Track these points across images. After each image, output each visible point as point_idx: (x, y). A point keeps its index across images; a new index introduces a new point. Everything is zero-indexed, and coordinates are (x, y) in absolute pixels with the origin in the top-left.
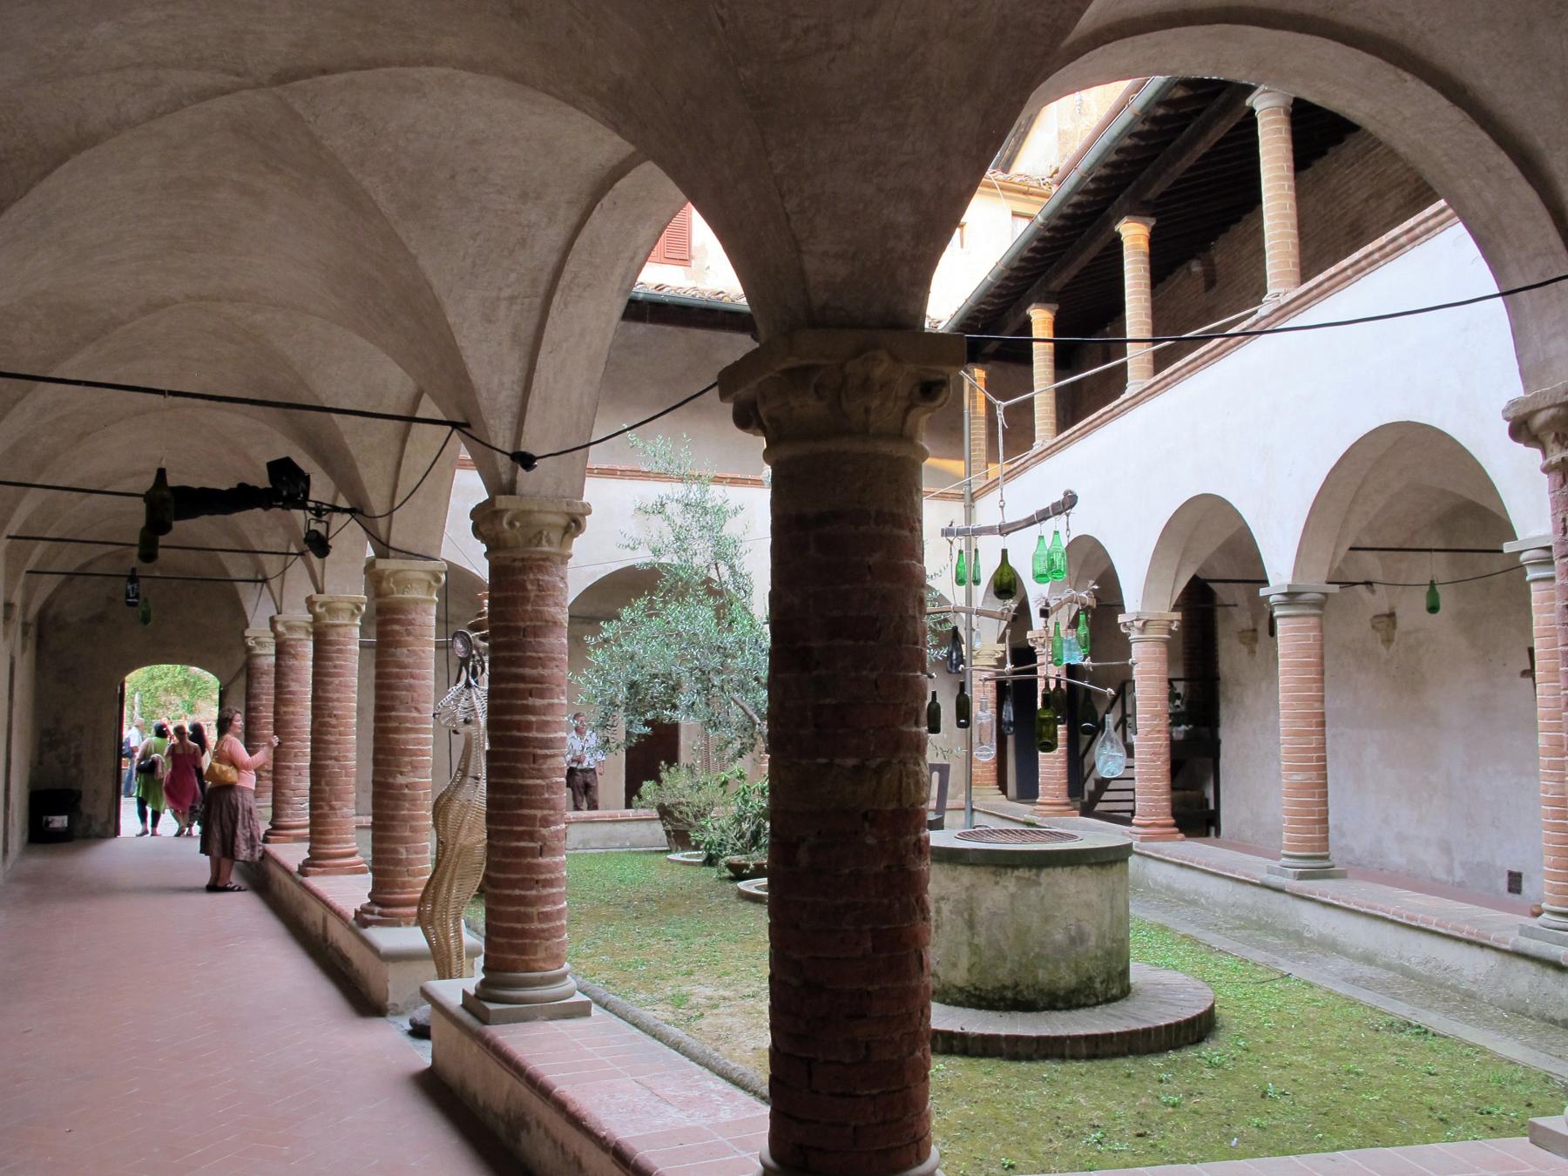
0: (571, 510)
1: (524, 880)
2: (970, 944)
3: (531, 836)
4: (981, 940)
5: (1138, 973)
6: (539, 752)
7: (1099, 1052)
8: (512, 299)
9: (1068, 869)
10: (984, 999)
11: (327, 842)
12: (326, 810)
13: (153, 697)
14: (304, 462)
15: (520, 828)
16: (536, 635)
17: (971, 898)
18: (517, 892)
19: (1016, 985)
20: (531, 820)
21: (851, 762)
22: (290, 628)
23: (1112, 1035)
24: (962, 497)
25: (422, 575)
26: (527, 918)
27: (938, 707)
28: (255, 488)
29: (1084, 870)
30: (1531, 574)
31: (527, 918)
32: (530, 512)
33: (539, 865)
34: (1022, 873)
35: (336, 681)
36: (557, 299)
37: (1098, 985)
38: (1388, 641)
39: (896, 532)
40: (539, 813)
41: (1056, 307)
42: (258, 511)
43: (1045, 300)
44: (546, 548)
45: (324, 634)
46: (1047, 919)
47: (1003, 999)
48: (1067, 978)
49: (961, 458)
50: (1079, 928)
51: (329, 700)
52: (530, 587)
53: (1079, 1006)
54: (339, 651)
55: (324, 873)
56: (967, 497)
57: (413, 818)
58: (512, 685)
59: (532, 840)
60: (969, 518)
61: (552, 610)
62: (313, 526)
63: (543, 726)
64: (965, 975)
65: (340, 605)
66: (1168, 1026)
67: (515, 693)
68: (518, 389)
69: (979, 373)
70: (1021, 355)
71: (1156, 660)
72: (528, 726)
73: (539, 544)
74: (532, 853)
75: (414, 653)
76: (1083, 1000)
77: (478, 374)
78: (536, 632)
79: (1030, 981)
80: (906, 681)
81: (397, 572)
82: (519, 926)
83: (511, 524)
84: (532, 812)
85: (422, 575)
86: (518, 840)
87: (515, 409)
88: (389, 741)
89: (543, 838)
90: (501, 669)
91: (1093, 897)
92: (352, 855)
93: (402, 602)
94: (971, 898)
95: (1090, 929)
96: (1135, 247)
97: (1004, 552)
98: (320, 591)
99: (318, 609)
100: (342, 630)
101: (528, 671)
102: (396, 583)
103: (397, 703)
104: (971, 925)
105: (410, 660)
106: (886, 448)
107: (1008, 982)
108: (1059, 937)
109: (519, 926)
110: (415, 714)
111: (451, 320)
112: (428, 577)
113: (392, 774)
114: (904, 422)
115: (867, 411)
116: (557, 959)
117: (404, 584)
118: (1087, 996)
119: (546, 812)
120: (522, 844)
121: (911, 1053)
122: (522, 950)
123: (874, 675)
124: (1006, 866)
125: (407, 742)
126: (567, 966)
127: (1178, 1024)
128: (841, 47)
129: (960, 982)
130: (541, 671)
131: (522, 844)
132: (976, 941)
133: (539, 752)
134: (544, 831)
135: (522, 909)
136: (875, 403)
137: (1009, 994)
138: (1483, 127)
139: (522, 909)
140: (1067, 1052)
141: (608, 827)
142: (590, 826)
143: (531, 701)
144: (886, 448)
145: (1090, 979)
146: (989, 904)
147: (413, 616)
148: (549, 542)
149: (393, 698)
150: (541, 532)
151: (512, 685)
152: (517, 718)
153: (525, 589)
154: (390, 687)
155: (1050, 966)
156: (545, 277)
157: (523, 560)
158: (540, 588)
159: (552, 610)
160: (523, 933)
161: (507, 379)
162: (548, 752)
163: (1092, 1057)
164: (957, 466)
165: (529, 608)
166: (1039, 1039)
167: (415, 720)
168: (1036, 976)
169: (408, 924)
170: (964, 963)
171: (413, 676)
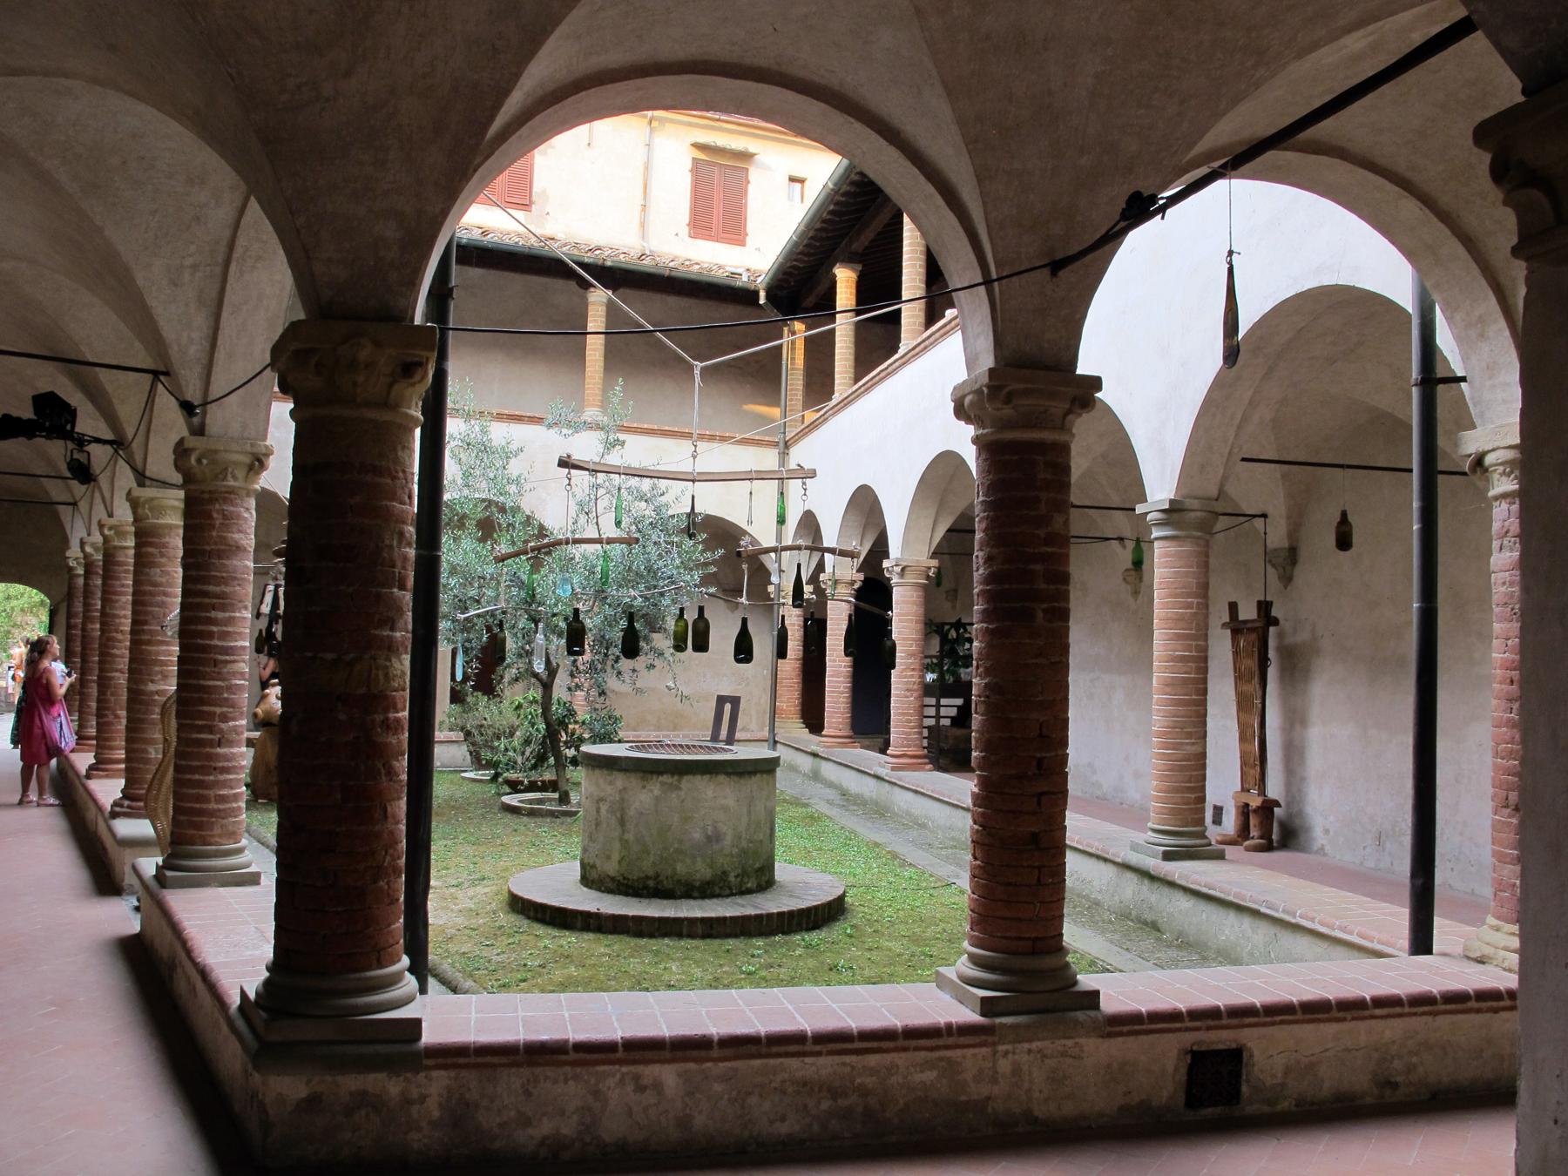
0: (255, 450)
1: (202, 767)
3: (211, 729)
4: (630, 837)
5: (782, 871)
8: (195, 267)
10: (632, 887)
12: (111, 718)
13: (9, 616)
14: (74, 398)
16: (220, 558)
17: (623, 800)
18: (197, 777)
19: (657, 875)
20: (212, 715)
21: (330, 656)
23: (725, 919)
24: (776, 444)
26: (206, 799)
28: (19, 419)
29: (722, 778)
30: (1156, 533)
31: (206, 799)
32: (216, 452)
33: (218, 755)
34: (666, 778)
36: (233, 267)
37: (732, 878)
38: (1136, 593)
39: (378, 480)
40: (218, 710)
42: (22, 439)
43: (849, 260)
44: (232, 483)
45: (113, 556)
46: (686, 820)
47: (646, 887)
48: (702, 871)
49: (778, 405)
51: (115, 616)
55: (107, 777)
58: (198, 600)
60: (782, 463)
61: (236, 536)
62: (76, 456)
63: (225, 635)
66: (781, 914)
67: (200, 607)
68: (207, 345)
70: (826, 305)
72: (211, 635)
73: (225, 478)
74: (211, 744)
75: (168, 573)
76: (717, 891)
77: (169, 332)
78: (220, 555)
79: (669, 872)
80: (378, 596)
83: (199, 461)
84: (212, 709)
87: (204, 362)
88: (142, 652)
89: (221, 731)
90: (190, 586)
91: (730, 802)
94: (623, 800)
95: (728, 831)
98: (111, 515)
99: (106, 532)
101: (211, 588)
102: (151, 509)
103: (149, 618)
104: (622, 822)
105: (164, 580)
106: (371, 414)
107: (651, 873)
108: (697, 835)
111: (140, 282)
113: (142, 682)
114: (389, 393)
115: (355, 384)
116: (233, 836)
121: (375, 882)
122: (200, 826)
123: (351, 589)
124: (652, 773)
125: (158, 653)
126: (244, 842)
127: (791, 913)
128: (328, 100)
129: (612, 873)
130: (224, 588)
132: (626, 836)
134: (223, 726)
136: (361, 379)
137: (651, 883)
138: (914, 164)
140: (685, 931)
143: (213, 614)
144: (371, 414)
145: (724, 873)
146: (637, 804)
148: (235, 478)
149: (146, 613)
151: (198, 600)
152: (200, 627)
153: (210, 517)
154: (143, 604)
156: (222, 249)
158: (225, 517)
159: (236, 536)
160: (201, 812)
161: (195, 335)
164: (776, 412)
166: (661, 919)
170: (616, 857)
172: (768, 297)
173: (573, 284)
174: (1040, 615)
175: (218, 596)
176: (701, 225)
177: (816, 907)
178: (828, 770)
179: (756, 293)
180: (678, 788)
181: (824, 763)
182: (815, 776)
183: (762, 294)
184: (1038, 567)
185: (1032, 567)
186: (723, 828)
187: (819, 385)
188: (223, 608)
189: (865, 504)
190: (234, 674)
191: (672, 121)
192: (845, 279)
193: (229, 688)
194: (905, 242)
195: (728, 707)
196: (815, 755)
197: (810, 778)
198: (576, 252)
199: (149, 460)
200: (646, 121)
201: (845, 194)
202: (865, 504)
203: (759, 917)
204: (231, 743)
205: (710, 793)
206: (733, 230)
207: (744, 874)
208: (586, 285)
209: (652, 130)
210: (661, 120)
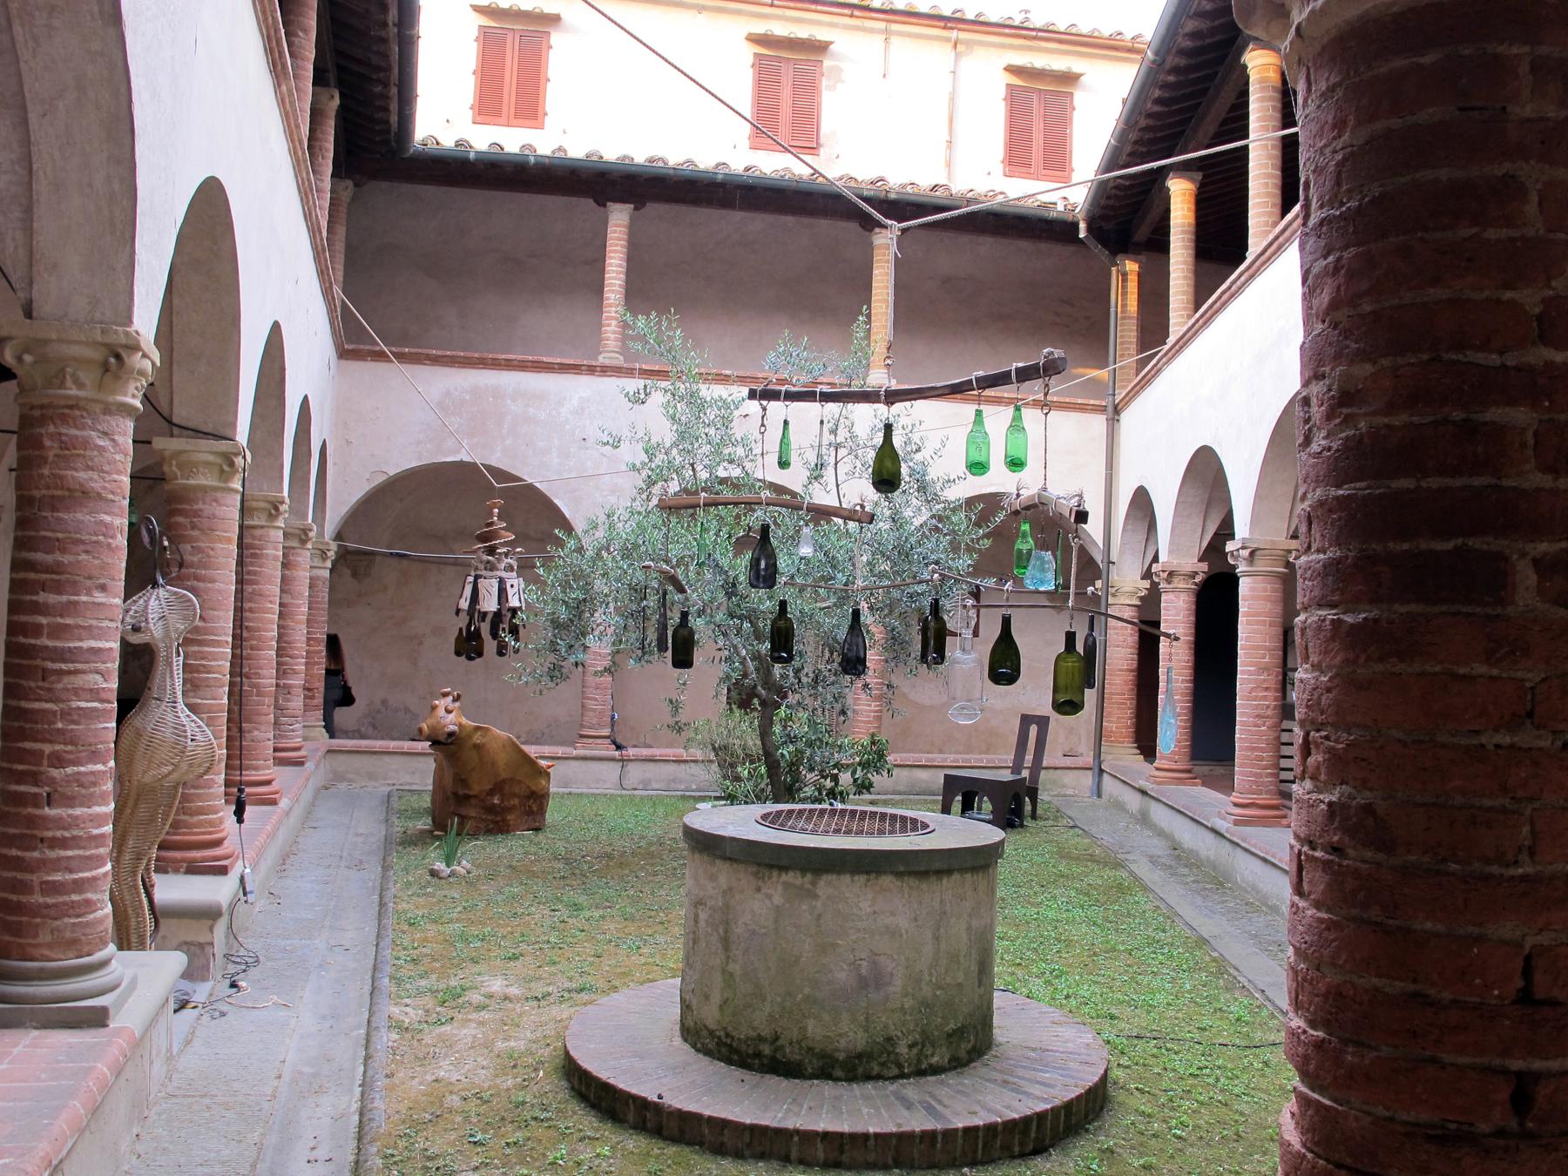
0: (107, 340)
1: (23, 836)
2: (724, 971)
5: (1018, 1018)
6: (50, 665)
7: (845, 1158)
9: (862, 879)
10: (737, 1051)
15: (20, 767)
16: (54, 509)
18: (14, 852)
23: (866, 1136)
24: (1101, 409)
25: (211, 458)
26: (25, 888)
27: (692, 633)
29: (887, 880)
31: (25, 888)
32: (46, 342)
33: (45, 818)
34: (791, 877)
37: (902, 1049)
40: (47, 748)
41: (1199, 176)
43: (1184, 168)
44: (74, 392)
47: (758, 1055)
48: (850, 1036)
52: (48, 443)
53: (868, 1077)
54: (254, 556)
56: (1110, 409)
59: (36, 784)
61: (82, 475)
63: (59, 631)
64: (717, 1014)
65: (255, 504)
66: (970, 1131)
69: (1131, 266)
71: (1266, 599)
72: (59, 631)
73: (62, 385)
74: (35, 801)
75: (199, 550)
76: (876, 1069)
79: (795, 1035)
81: (181, 452)
82: (14, 898)
85: (211, 458)
86: (18, 783)
89: (53, 781)
92: (268, 783)
93: (187, 488)
96: (1262, 80)
97: (888, 428)
100: (258, 532)
101: (39, 556)
102: (179, 466)
104: (726, 942)
105: (195, 559)
107: (766, 1032)
108: (842, 975)
109: (14, 898)
112: (219, 460)
117: (189, 467)
118: (883, 1064)
119: (58, 747)
120: (22, 788)
122: (17, 930)
124: (771, 867)
127: (991, 1129)
130: (58, 556)
131: (22, 788)
132: (731, 967)
133: (50, 665)
135: (19, 876)
137: (766, 1050)
139: (19, 876)
140: (794, 1154)
141: (672, 768)
142: (651, 766)
143: (42, 597)
145: (889, 1039)
147: (200, 506)
150: (63, 370)
153: (41, 446)
155: (826, 1017)
157: (42, 407)
158: (64, 446)
159: (82, 475)
160: (19, 908)
162: (71, 666)
165: (46, 472)
169: (177, 871)
170: (716, 998)
171: (197, 578)
172: (1089, 229)
173: (853, 227)
174: (1526, 577)
175: (48, 569)
176: (1016, 159)
177: (1041, 1116)
178: (1159, 814)
179: (1075, 225)
180: (816, 897)
181: (1153, 804)
182: (1144, 819)
183: (1082, 226)
184: (1521, 416)
185: (1494, 414)
187: (1153, 330)
188: (58, 588)
189: (1205, 471)
190: (77, 692)
191: (981, 44)
192: (1181, 195)
193: (66, 714)
194: (1252, 118)
196: (1144, 792)
197: (1137, 821)
198: (853, 184)
199: (176, 402)
200: (950, 46)
201: (1175, 70)
202: (1205, 471)
203: (929, 1137)
204: (88, 801)
205: (866, 906)
206: (1057, 162)
207: (925, 1041)
208: (869, 224)
209: (958, 56)
210: (968, 43)
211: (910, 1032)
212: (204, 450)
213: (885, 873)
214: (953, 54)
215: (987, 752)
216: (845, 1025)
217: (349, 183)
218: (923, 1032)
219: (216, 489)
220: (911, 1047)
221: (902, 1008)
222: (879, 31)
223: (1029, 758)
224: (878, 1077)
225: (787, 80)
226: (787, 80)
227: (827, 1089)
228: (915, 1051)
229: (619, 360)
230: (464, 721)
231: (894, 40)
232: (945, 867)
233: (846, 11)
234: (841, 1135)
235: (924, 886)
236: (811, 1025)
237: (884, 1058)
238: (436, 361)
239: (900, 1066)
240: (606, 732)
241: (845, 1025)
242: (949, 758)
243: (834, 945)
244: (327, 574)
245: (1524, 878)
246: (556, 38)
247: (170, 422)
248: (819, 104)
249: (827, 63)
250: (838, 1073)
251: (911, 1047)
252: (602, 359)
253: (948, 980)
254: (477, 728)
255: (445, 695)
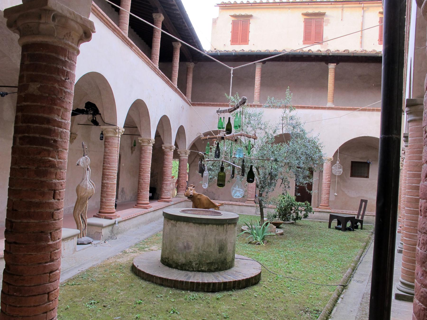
7: (164, 284)
9: (185, 223)
11: (139, 200)
22: (166, 148)
23: (168, 279)
25: (112, 130)
29: (191, 224)
35: (143, 160)
37: (194, 264)
46: (177, 239)
48: (182, 260)
50: (188, 244)
53: (185, 270)
54: (145, 152)
55: (137, 208)
57: (107, 191)
65: (145, 140)
75: (109, 150)
79: (171, 258)
81: (106, 129)
91: (195, 234)
97: (229, 118)
100: (146, 147)
102: (106, 132)
108: (181, 245)
110: (109, 165)
117: (107, 132)
118: (189, 267)
125: (106, 172)
137: (167, 260)
145: (190, 262)
155: (177, 255)
163: (161, 285)
167: (108, 167)
168: (173, 257)
169: (102, 218)
171: (109, 156)
180: (176, 226)
186: (191, 244)
195: (364, 203)
207: (200, 263)
210: (368, 7)
211: (196, 261)
212: (110, 128)
213: (190, 222)
214: (362, 11)
215: (371, 211)
216: (181, 257)
217: (193, 63)
218: (199, 261)
219: (113, 136)
220: (196, 264)
221: (194, 255)
222: (340, 8)
223: (362, 212)
224: (188, 270)
225: (314, 26)
226: (314, 26)
227: (175, 270)
228: (197, 265)
229: (258, 103)
230: (195, 192)
231: (345, 9)
232: (206, 222)
233: (330, 3)
234: (163, 278)
235: (201, 227)
236: (174, 256)
237: (189, 266)
238: (204, 105)
239: (193, 268)
240: (253, 199)
241: (181, 257)
242: (332, 211)
243: (179, 238)
244: (187, 158)
245: (14, 190)
246: (252, 21)
247: (104, 122)
248: (323, 30)
249: (325, 18)
250: (179, 268)
251: (196, 264)
252: (254, 103)
253: (207, 250)
254: (199, 194)
255: (191, 186)
